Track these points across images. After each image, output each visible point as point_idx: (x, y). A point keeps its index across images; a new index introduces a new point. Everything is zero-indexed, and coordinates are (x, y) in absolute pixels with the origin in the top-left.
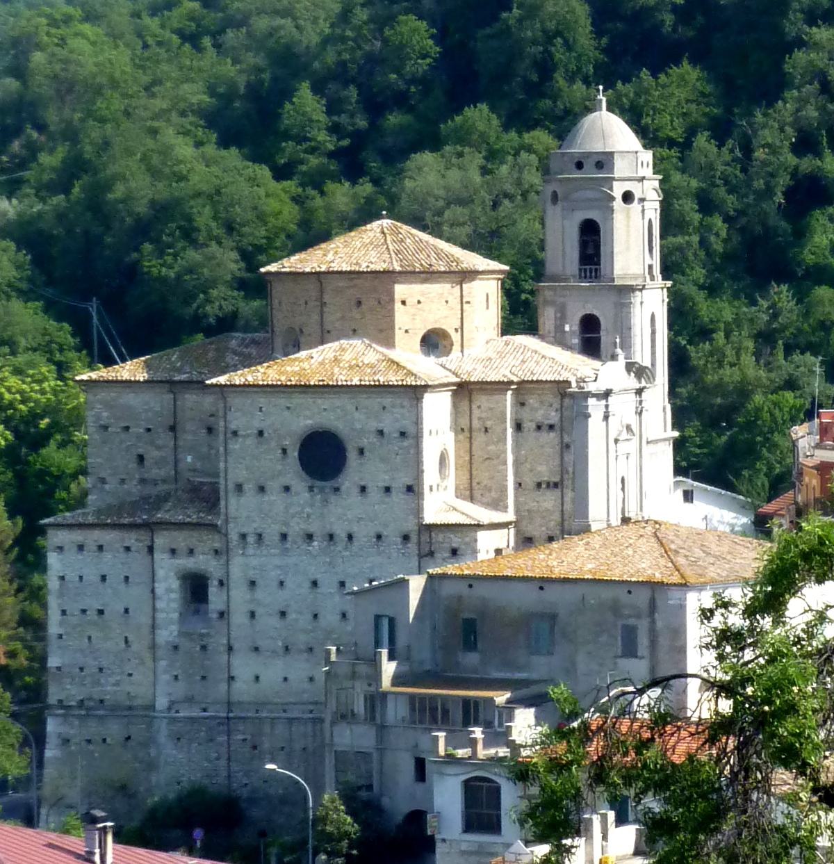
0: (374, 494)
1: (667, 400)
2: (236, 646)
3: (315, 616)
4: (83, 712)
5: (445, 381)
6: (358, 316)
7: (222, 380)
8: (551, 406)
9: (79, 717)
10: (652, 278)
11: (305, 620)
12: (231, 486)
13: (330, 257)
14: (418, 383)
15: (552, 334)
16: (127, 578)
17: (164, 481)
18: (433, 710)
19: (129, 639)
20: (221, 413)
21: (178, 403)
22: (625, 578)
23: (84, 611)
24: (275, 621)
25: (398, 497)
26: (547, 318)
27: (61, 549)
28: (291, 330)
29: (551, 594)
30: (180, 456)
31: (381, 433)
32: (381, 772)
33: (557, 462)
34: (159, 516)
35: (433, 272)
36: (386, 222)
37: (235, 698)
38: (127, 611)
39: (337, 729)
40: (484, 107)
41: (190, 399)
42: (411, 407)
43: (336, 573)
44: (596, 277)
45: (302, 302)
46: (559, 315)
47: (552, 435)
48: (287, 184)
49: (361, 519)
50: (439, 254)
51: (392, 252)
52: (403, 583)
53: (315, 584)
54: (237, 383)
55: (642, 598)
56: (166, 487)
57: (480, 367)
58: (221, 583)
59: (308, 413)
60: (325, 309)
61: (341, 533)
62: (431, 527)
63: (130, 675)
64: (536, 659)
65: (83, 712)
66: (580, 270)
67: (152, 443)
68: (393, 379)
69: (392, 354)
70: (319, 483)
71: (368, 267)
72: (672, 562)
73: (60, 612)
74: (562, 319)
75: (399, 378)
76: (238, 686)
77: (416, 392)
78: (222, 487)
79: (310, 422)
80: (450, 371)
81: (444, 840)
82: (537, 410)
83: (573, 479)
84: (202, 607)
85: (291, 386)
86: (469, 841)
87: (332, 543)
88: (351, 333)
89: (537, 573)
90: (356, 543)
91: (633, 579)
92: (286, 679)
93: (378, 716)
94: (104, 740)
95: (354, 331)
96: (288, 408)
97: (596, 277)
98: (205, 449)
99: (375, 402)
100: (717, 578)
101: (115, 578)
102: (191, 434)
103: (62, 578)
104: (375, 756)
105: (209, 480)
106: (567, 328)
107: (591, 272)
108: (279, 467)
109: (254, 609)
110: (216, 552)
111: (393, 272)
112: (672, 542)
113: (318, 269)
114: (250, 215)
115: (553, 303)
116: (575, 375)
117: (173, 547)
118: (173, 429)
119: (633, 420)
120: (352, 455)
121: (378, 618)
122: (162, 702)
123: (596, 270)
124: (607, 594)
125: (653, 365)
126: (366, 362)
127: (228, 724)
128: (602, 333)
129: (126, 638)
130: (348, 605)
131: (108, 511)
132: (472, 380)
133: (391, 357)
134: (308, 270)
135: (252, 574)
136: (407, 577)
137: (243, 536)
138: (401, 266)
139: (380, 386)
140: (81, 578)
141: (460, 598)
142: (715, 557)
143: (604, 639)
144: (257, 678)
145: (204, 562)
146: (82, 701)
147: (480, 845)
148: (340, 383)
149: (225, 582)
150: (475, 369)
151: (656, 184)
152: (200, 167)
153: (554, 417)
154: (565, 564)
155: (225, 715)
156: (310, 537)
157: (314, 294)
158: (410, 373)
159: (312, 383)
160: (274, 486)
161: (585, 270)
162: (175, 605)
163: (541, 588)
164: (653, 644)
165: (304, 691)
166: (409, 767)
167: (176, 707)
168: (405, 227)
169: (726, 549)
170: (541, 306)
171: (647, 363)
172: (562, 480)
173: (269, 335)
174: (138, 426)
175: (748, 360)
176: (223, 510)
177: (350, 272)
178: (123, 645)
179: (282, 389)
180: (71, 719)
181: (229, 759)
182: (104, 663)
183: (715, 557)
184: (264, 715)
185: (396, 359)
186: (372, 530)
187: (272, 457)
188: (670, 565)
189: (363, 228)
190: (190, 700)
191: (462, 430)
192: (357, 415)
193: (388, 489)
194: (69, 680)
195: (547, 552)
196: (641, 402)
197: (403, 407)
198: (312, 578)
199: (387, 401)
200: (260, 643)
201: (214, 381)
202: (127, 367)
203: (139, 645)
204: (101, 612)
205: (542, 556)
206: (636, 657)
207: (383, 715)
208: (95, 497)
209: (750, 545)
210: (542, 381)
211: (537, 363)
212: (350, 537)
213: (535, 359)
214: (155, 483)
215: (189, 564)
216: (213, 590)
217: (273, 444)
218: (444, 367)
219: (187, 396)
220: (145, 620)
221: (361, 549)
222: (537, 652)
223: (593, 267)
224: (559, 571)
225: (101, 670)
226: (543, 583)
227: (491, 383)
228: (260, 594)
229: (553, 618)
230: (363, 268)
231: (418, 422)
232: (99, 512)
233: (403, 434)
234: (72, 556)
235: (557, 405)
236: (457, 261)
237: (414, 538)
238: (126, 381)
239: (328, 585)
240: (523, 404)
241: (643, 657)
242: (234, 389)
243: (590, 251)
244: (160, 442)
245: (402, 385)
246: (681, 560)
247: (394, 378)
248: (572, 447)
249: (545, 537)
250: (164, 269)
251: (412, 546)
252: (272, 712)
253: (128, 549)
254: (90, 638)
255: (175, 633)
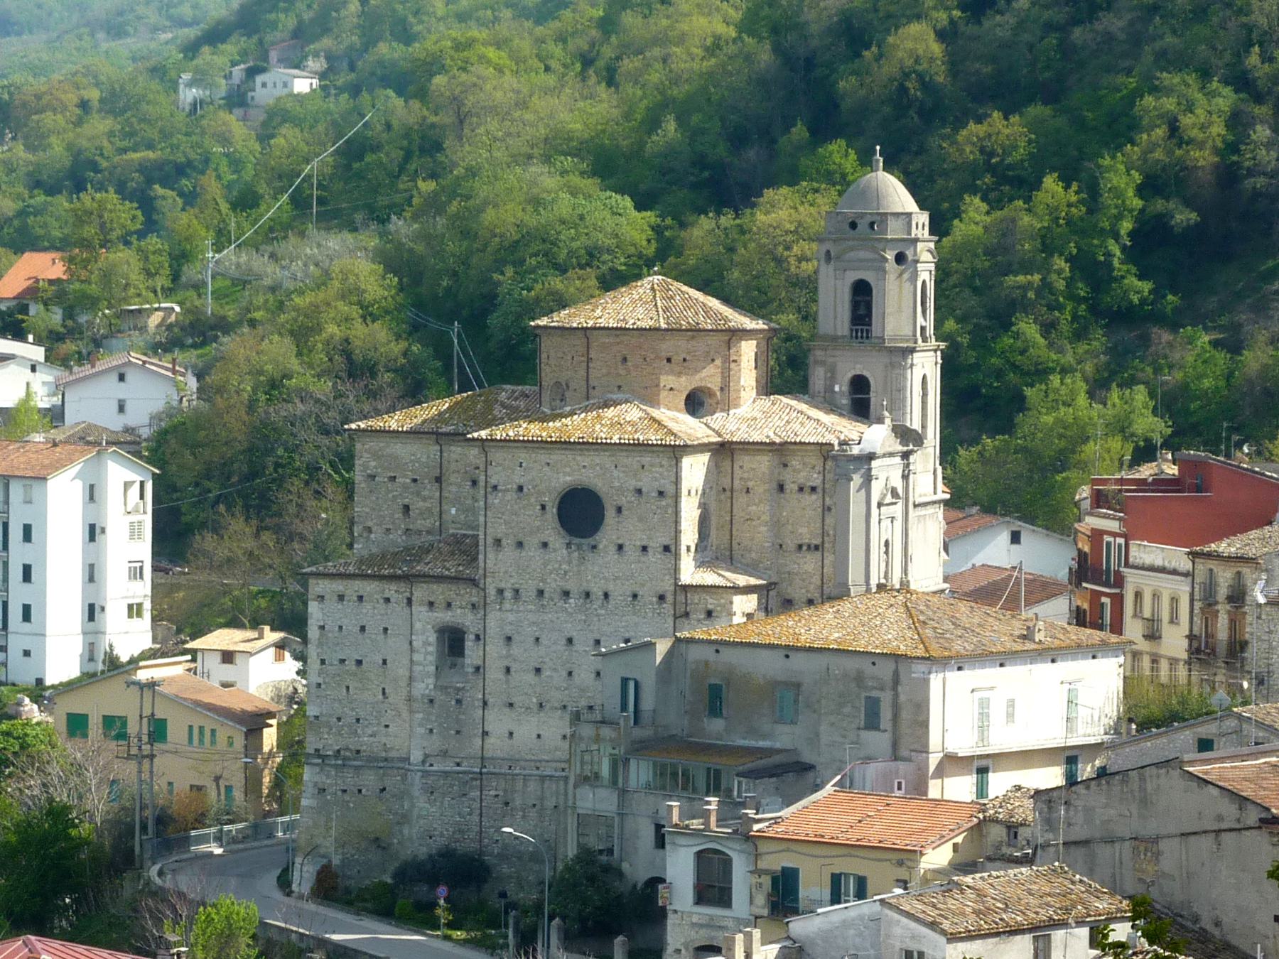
0: (631, 553)
1: (938, 462)
2: (491, 700)
3: (570, 674)
4: (340, 762)
5: (705, 440)
6: (623, 372)
7: (483, 434)
8: (813, 468)
9: (336, 766)
10: (925, 340)
11: (559, 678)
12: (490, 540)
13: (598, 312)
14: (677, 443)
15: (822, 394)
16: (386, 630)
17: (428, 532)
18: (674, 775)
19: (387, 691)
20: (482, 467)
21: (445, 454)
22: (870, 649)
23: (342, 661)
24: (530, 678)
25: (654, 557)
26: (818, 377)
27: (321, 598)
28: (558, 384)
29: (798, 661)
30: (445, 507)
31: (639, 491)
32: (621, 838)
33: (819, 525)
34: (418, 568)
35: (700, 330)
36: (657, 279)
37: (488, 754)
38: (385, 662)
39: (578, 791)
40: (842, 143)
41: (455, 451)
42: (670, 466)
43: (592, 631)
44: (867, 337)
45: (569, 358)
46: (829, 375)
47: (814, 497)
48: (644, 214)
49: (617, 578)
50: (707, 310)
51: (660, 310)
52: (650, 646)
53: (570, 641)
54: (498, 438)
55: (885, 671)
56: (431, 538)
57: (744, 427)
58: (478, 638)
59: (568, 470)
60: (590, 365)
61: (597, 592)
62: (686, 588)
63: (387, 726)
64: (780, 728)
65: (340, 762)
66: (852, 330)
67: (418, 494)
68: (653, 438)
69: (655, 413)
70: (576, 540)
71: (634, 324)
72: (918, 634)
73: (319, 662)
74: (832, 378)
75: (658, 437)
76: (490, 741)
77: (677, 452)
78: (481, 543)
79: (568, 478)
80: (714, 430)
81: (675, 912)
82: (799, 471)
83: (834, 542)
84: (460, 660)
85: (551, 442)
86: (700, 914)
87: (588, 601)
88: (616, 389)
89: (784, 641)
90: (612, 602)
91: (878, 651)
92: (539, 736)
93: (620, 780)
94: (360, 791)
95: (619, 387)
96: (548, 464)
97: (867, 337)
98: (469, 502)
99: (632, 461)
100: (962, 651)
101: (374, 629)
102: (456, 484)
103: (322, 628)
104: (616, 820)
105: (471, 532)
106: (837, 388)
107: (862, 333)
108: (538, 523)
109: (509, 665)
110: (473, 605)
111: (658, 329)
112: (922, 612)
113: (585, 325)
114: (611, 242)
115: (823, 363)
116: (838, 438)
117: (432, 599)
118: (438, 480)
119: (898, 484)
120: (610, 514)
121: (625, 681)
122: (416, 756)
123: (867, 331)
124: (851, 664)
125: (924, 427)
126: (628, 419)
127: (481, 779)
128: (872, 394)
129: (384, 689)
130: (598, 663)
131: (370, 560)
132: (734, 440)
133: (654, 415)
134: (575, 325)
135: (508, 630)
136: (653, 641)
137: (500, 592)
138: (668, 324)
139: (639, 444)
140: (341, 627)
141: (707, 663)
142: (965, 629)
143: (847, 710)
144: (511, 734)
145: (461, 617)
146: (339, 751)
147: (711, 918)
148: (599, 441)
149: (482, 637)
150: (739, 429)
151: (932, 245)
152: (565, 196)
153: (816, 480)
154: (812, 632)
155: (478, 770)
156: (566, 594)
157: (583, 350)
158: (671, 432)
159: (572, 440)
160: (532, 542)
161: (862, 330)
162: (431, 658)
163: (787, 656)
164: (896, 717)
165: (557, 749)
166: (648, 833)
167: (430, 760)
168: (675, 283)
169: (976, 620)
170: (811, 365)
171: (916, 425)
172: (823, 542)
173: (537, 388)
174: (405, 476)
175: (1082, 400)
176: (481, 564)
177: (617, 329)
178: (381, 697)
179: (543, 445)
180: (328, 768)
181: (481, 815)
182: (362, 714)
183: (965, 629)
184: (517, 772)
185: (657, 417)
186: (629, 588)
187: (531, 512)
188: (916, 637)
189: (634, 284)
190: (444, 754)
191: (724, 490)
192: (616, 473)
193: (645, 549)
194: (326, 730)
195: (796, 619)
196: (908, 465)
197: (662, 466)
198: (568, 635)
199: (647, 459)
200: (514, 700)
201: (475, 435)
202: (396, 417)
203: (397, 698)
204: (359, 662)
205: (790, 623)
206: (879, 730)
207: (626, 779)
208: (360, 546)
209: (1002, 617)
210: (804, 443)
211: (802, 424)
212: (606, 595)
213: (800, 419)
214: (419, 532)
215: (447, 617)
216: (469, 644)
217: (533, 500)
218: (708, 427)
219: (453, 448)
220: (403, 672)
221: (616, 608)
222: (780, 720)
223: (865, 328)
224: (805, 639)
225: (358, 720)
226: (789, 650)
227: (753, 443)
228: (516, 650)
229: (798, 686)
230: (629, 326)
231: (677, 481)
232: (361, 561)
233: (661, 493)
234: (332, 604)
235: (819, 468)
236: (726, 320)
237: (670, 598)
238: (394, 431)
239: (583, 645)
240: (785, 465)
241: (886, 731)
242: (494, 444)
243: (862, 312)
244: (426, 493)
245: (661, 445)
246: (929, 632)
247: (654, 438)
248: (833, 510)
249: (804, 600)
250: (525, 292)
251: (668, 607)
252: (525, 769)
253: (387, 600)
254: (348, 688)
255: (431, 687)
